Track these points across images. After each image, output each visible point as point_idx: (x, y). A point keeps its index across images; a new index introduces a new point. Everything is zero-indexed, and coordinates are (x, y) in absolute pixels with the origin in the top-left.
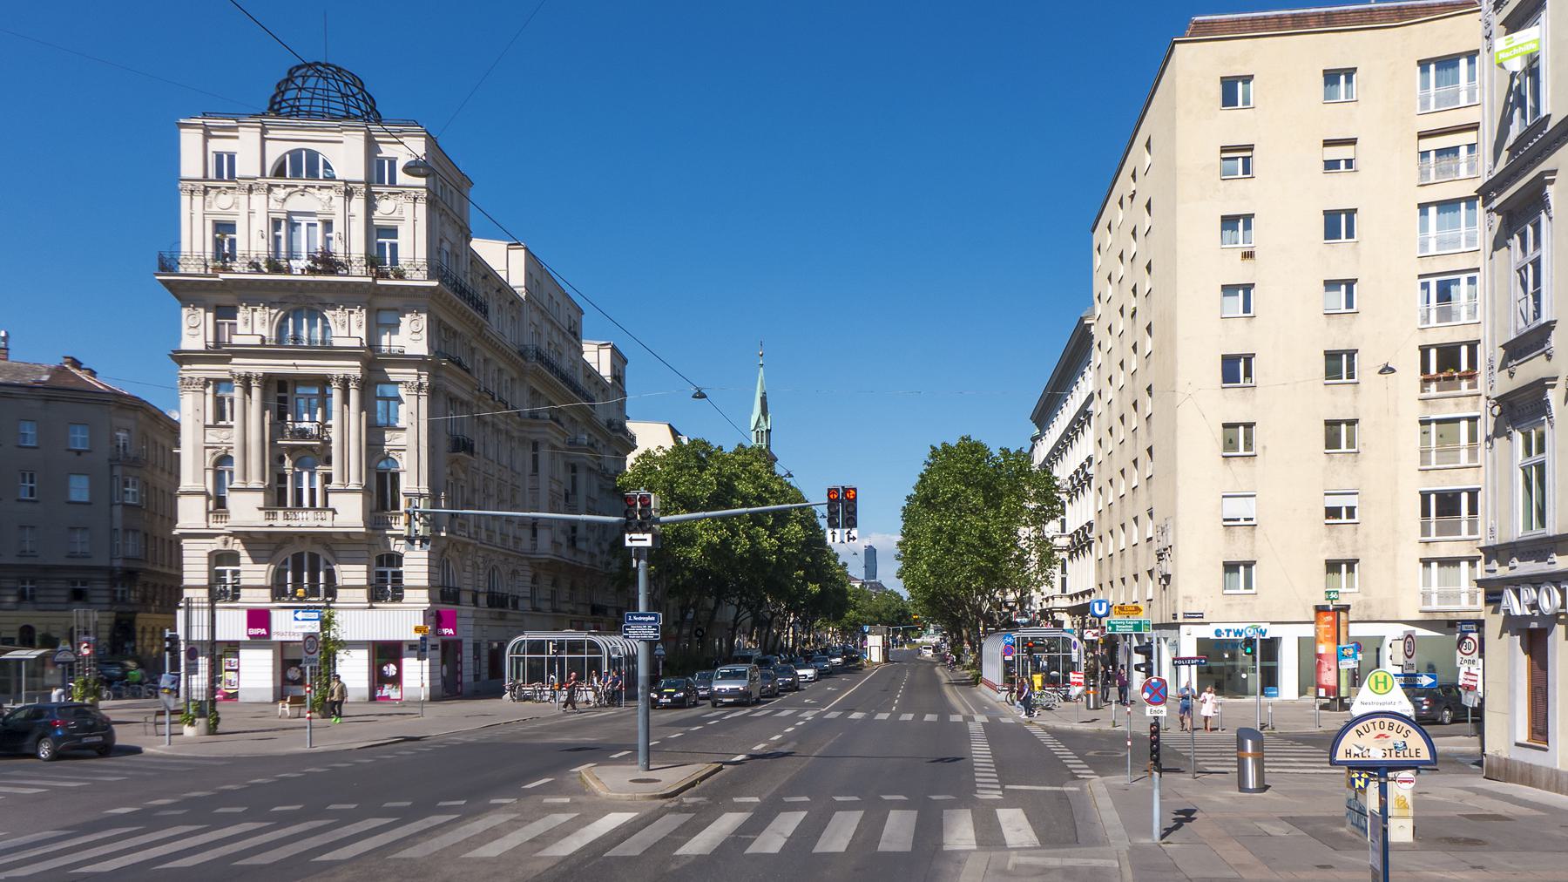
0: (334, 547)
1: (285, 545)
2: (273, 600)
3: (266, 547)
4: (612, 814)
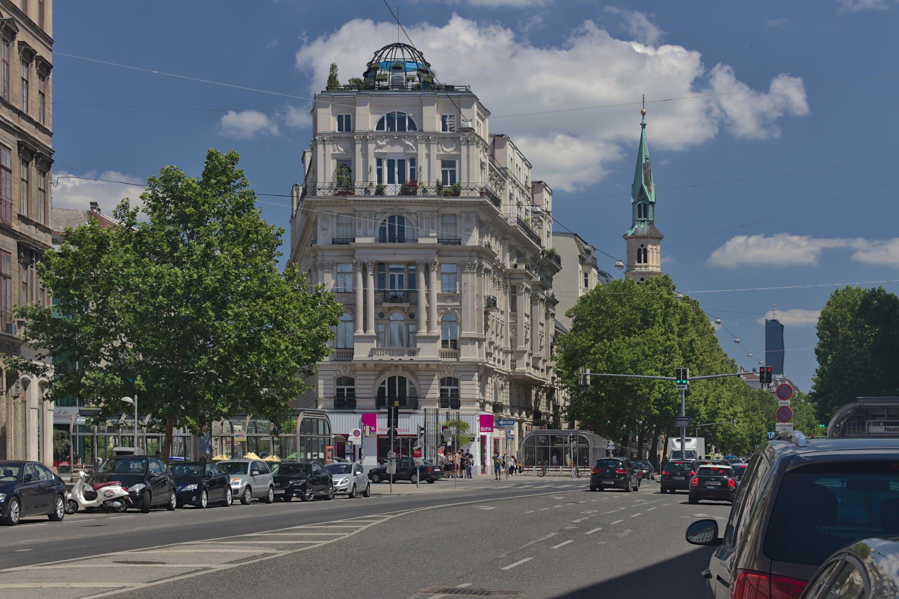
3: (373, 373)
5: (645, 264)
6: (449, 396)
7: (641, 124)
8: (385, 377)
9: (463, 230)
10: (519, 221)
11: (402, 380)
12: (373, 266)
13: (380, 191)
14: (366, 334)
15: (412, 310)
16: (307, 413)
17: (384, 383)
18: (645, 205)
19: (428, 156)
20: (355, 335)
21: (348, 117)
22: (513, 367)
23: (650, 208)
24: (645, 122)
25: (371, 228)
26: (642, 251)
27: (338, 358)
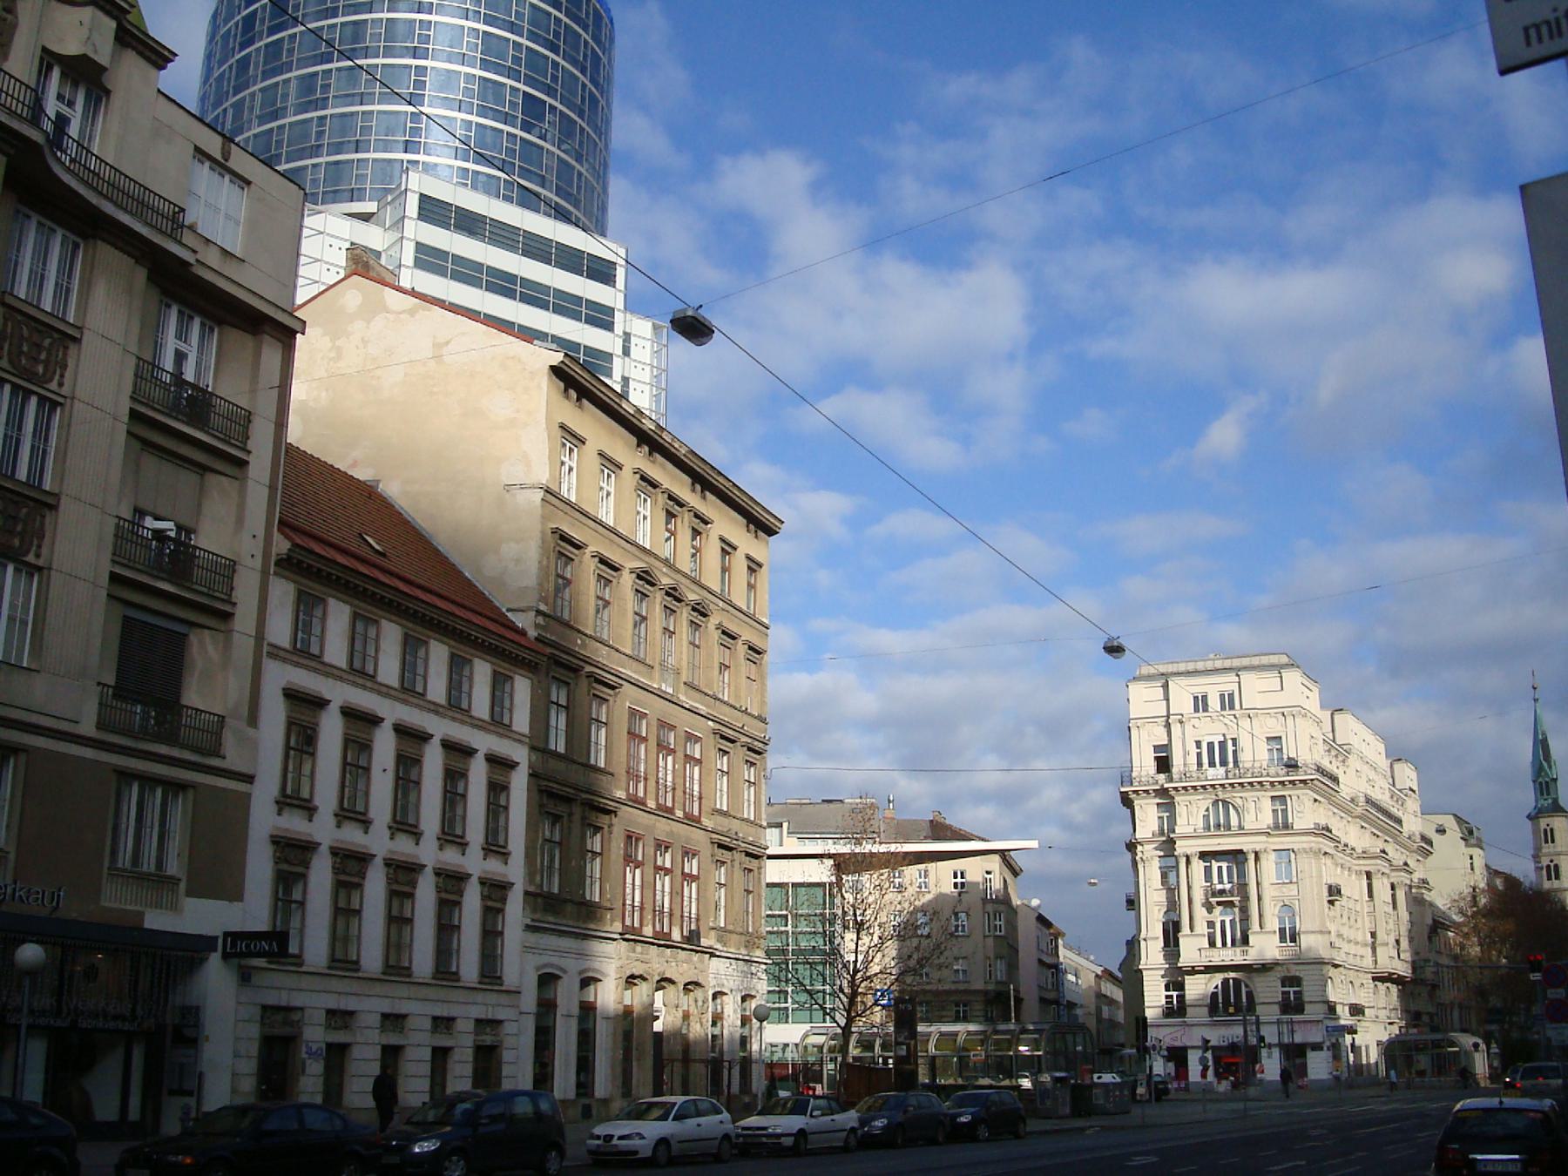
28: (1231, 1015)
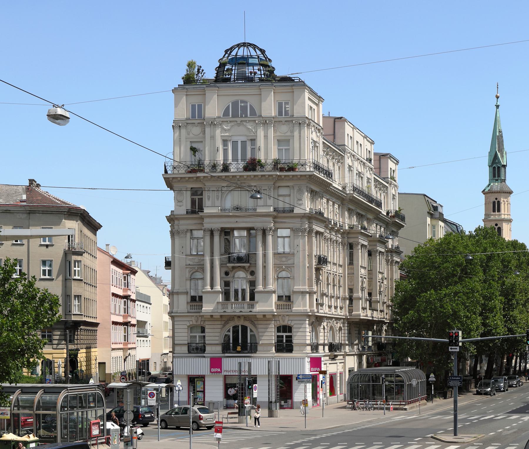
0: (256, 322)
1: (230, 322)
2: (223, 352)
3: (219, 323)
4: (490, 447)
5: (498, 213)
6: (284, 341)
7: (496, 105)
8: (230, 326)
9: (296, 200)
10: (355, 189)
11: (244, 328)
12: (219, 232)
13: (226, 168)
14: (213, 290)
15: (252, 269)
16: (70, 390)
17: (229, 331)
18: (499, 168)
19: (266, 137)
20: (203, 291)
21: (200, 106)
22: (351, 311)
23: (503, 169)
24: (498, 104)
25: (218, 199)
26: (496, 202)
27: (191, 311)
28: (239, 352)
